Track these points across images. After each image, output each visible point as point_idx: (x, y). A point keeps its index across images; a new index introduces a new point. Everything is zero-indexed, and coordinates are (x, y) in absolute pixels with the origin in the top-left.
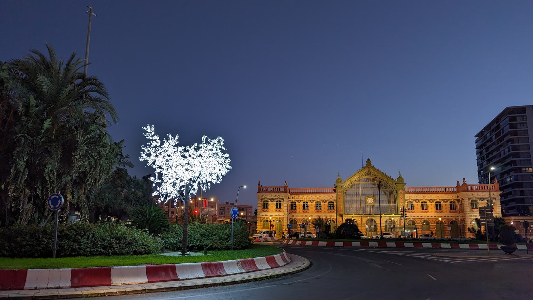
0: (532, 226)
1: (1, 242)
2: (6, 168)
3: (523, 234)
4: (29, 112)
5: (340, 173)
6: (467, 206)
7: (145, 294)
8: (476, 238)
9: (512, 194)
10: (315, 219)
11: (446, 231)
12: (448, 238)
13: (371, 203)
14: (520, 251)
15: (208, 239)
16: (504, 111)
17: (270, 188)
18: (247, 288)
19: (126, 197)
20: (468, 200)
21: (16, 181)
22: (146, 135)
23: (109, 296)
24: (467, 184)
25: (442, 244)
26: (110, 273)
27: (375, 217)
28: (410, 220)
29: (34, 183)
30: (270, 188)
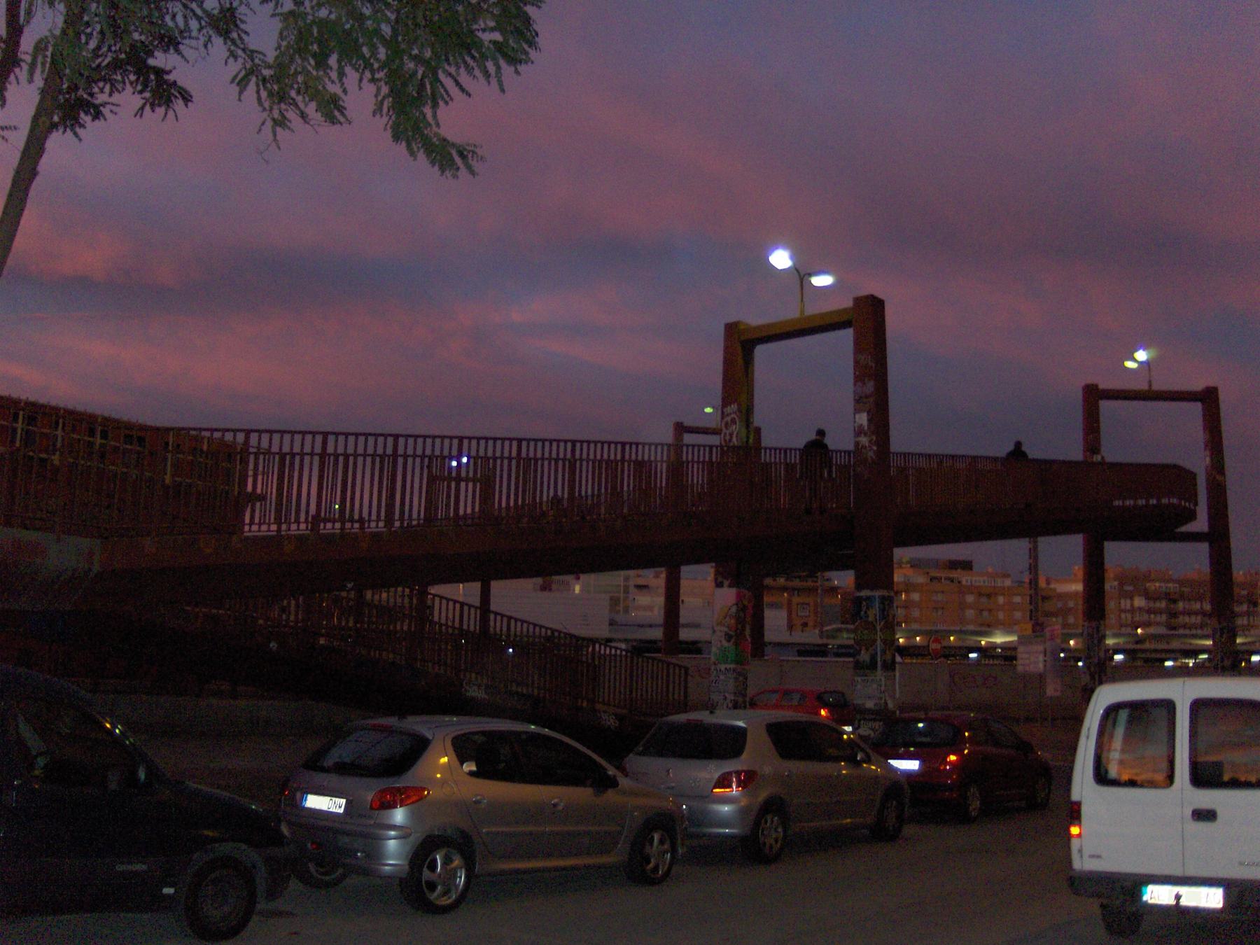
0: (1255, 658)
1: (228, 2)
2: (467, 545)
3: (1121, 762)
4: (422, 108)
5: (257, 130)
6: (377, 597)
7: (999, 583)
8: (165, 76)
9: (893, 597)
10: (10, 396)
11: (657, 699)
12: (1115, 644)
13: (109, 773)
14: (804, 296)
15: (30, 832)
16: (1089, 879)
17: (511, 442)
18: (604, 672)
19: (735, 693)
20: (1055, 632)
21: (302, 18)
22: (643, 661)
23: (298, 607)
24: (1030, 456)
25: (480, 586)
26: (43, 144)
27: (255, 88)
28: (878, 623)
29: (315, 34)
30: (511, 442)
